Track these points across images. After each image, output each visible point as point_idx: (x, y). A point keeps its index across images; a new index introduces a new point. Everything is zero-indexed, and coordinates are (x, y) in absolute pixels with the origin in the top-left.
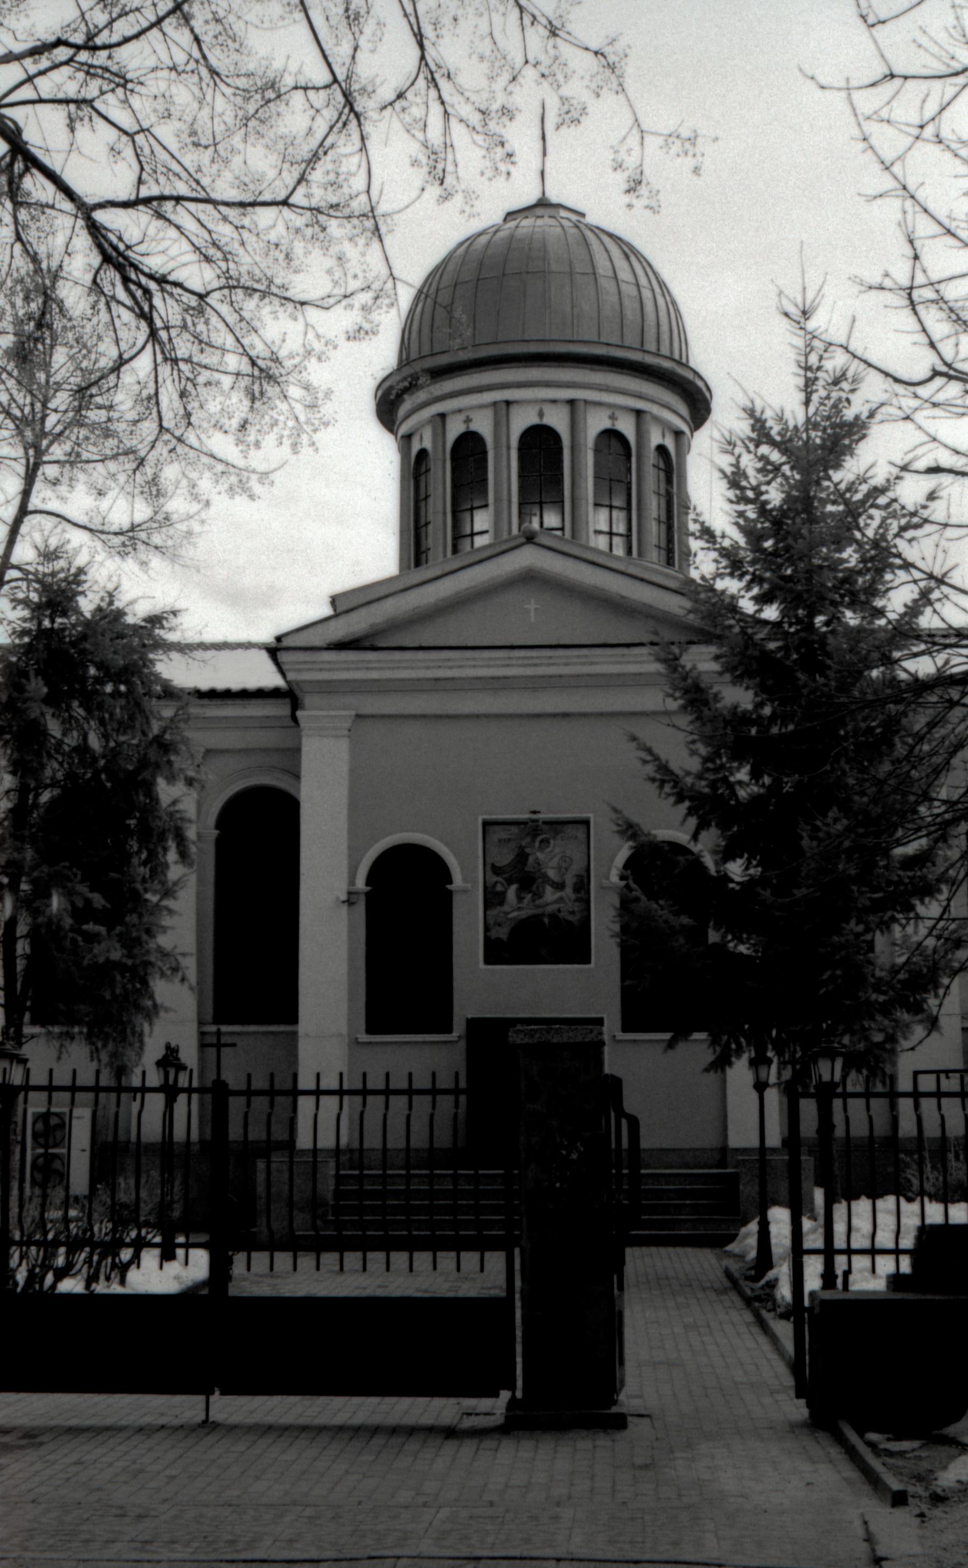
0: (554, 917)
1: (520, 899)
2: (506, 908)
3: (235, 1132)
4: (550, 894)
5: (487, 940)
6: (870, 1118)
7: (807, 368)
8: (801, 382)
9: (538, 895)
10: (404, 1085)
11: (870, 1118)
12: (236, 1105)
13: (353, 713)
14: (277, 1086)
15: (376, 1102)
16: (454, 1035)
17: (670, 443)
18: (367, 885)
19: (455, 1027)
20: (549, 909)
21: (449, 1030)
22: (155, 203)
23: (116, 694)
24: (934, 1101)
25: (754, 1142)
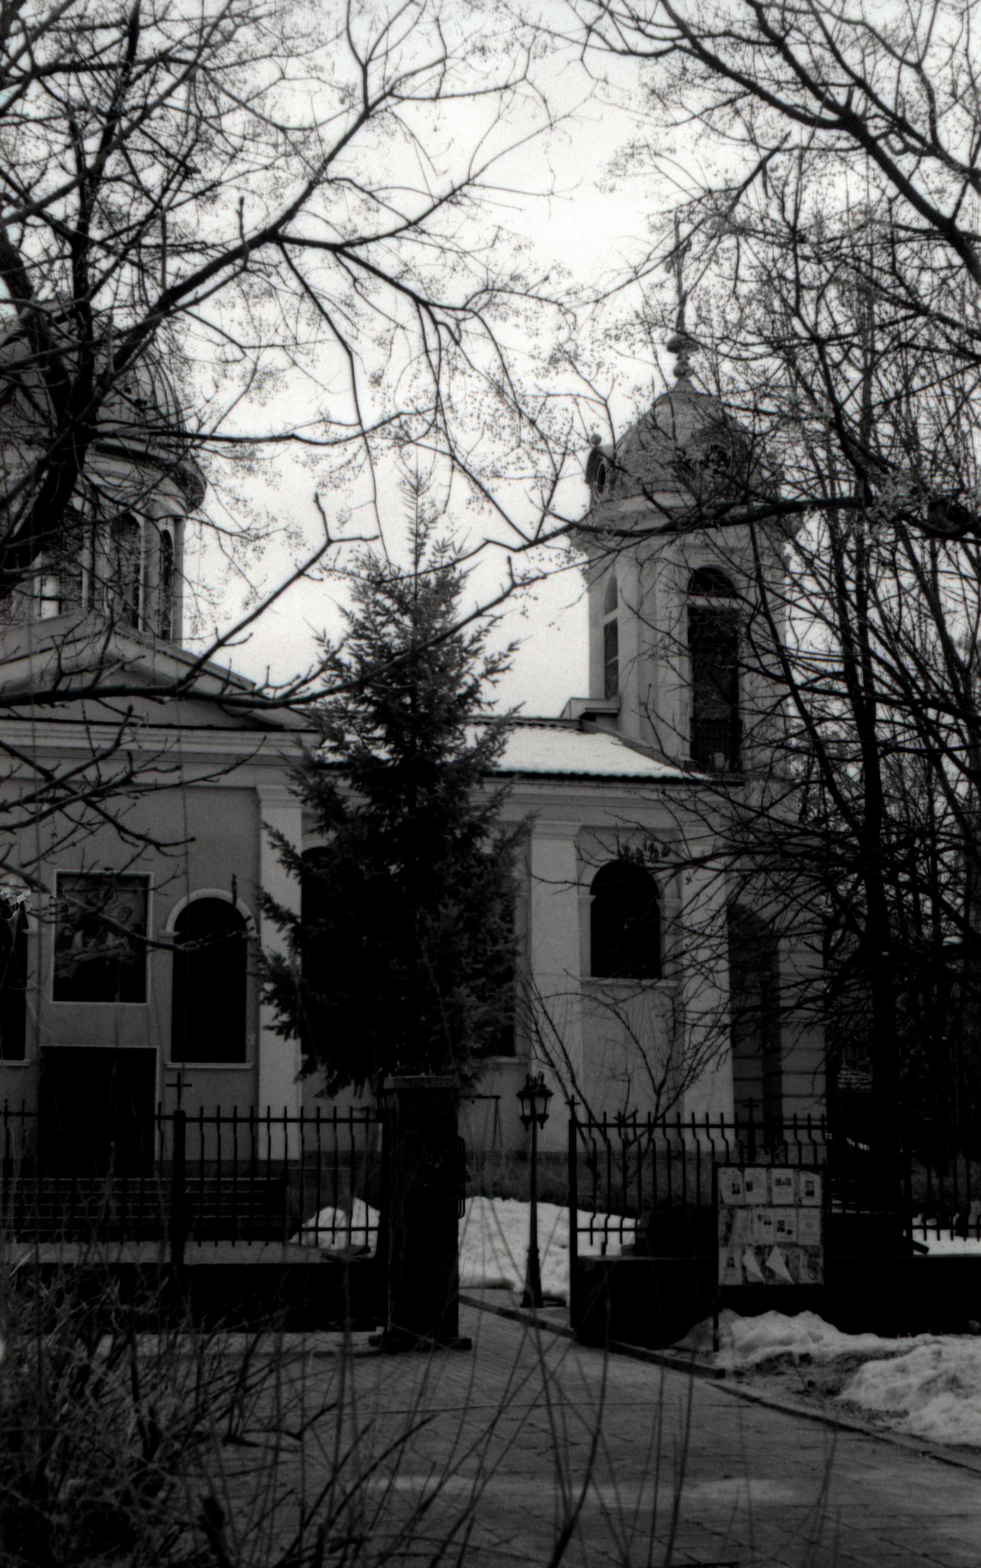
0: (114, 959)
1: (85, 944)
2: (73, 951)
3: (192, 1153)
4: (111, 940)
5: (56, 977)
6: (353, 1138)
7: (417, 535)
8: (412, 545)
9: (102, 940)
10: (231, 1115)
11: (353, 1138)
12: (191, 1130)
13: (579, 824)
14: (222, 1115)
15: (226, 1128)
16: (26, 1062)
17: (171, 529)
18: (176, 929)
19: (27, 1052)
20: (110, 954)
21: (22, 1057)
22: (67, 60)
23: (898, 834)
24: (214, 1125)
25: (282, 1157)
